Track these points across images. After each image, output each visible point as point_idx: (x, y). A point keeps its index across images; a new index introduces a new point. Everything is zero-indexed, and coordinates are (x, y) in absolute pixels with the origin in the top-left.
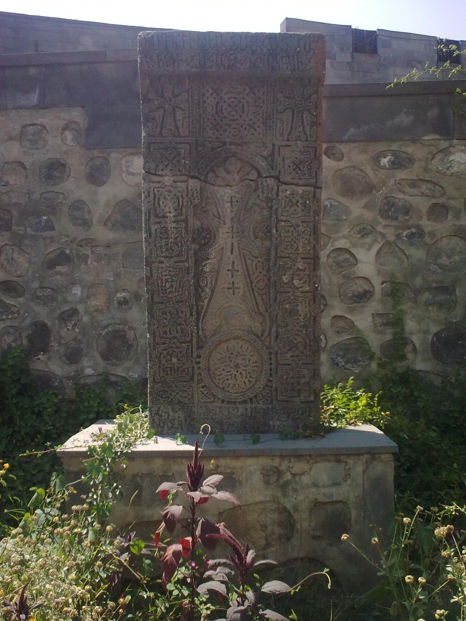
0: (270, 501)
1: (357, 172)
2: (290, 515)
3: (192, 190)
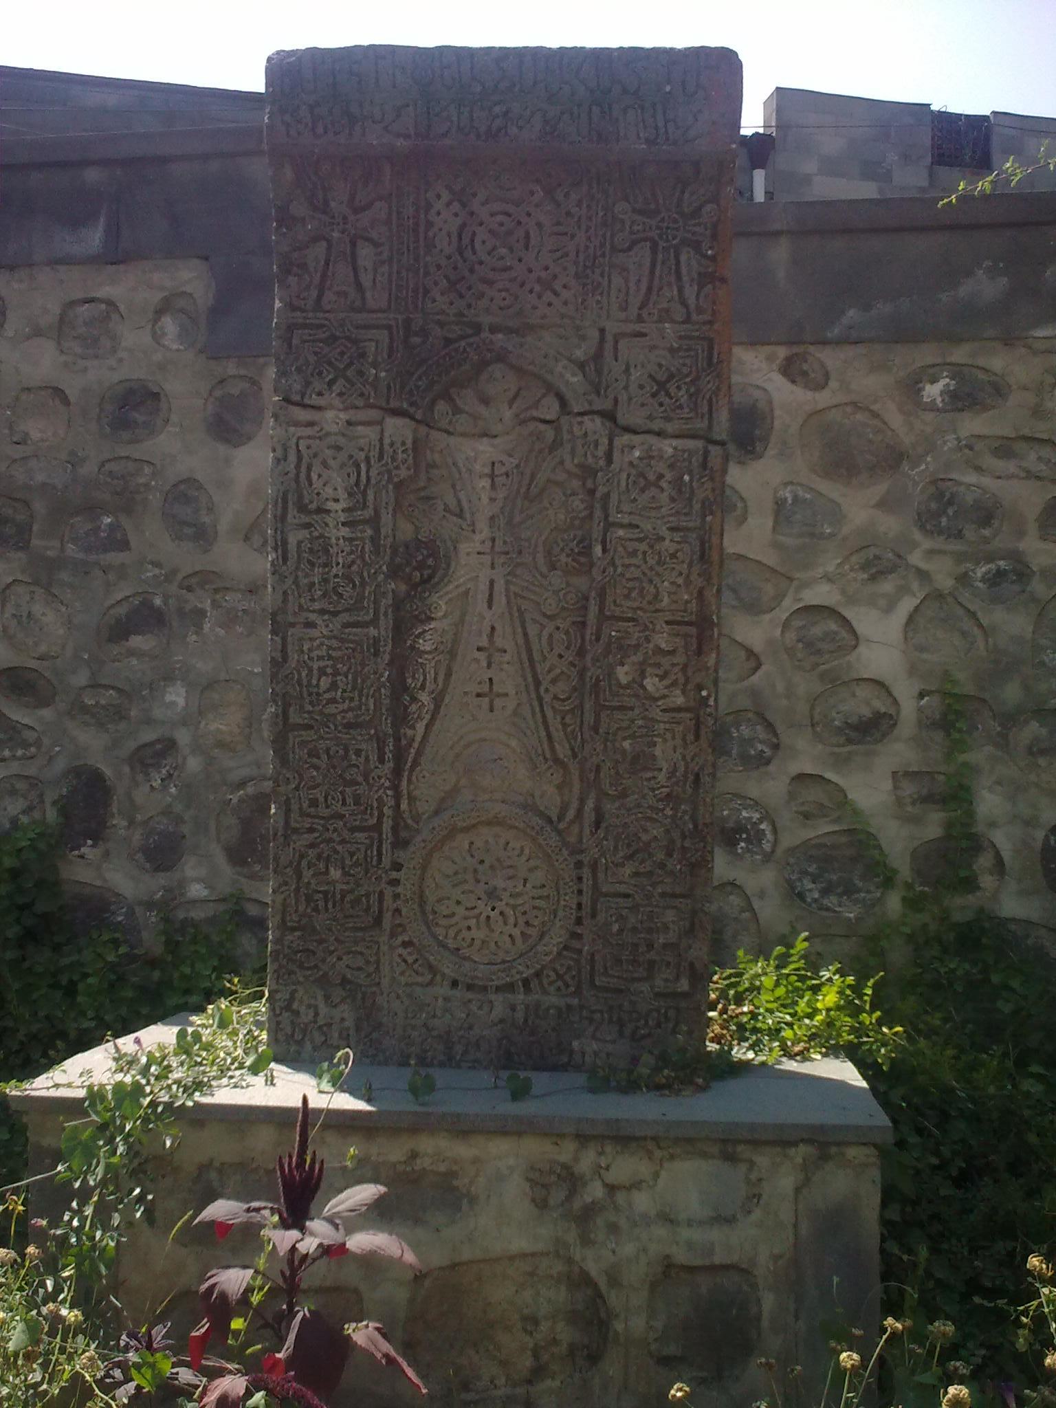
0: (547, 1254)
1: (859, 417)
2: (600, 1295)
3: (392, 445)
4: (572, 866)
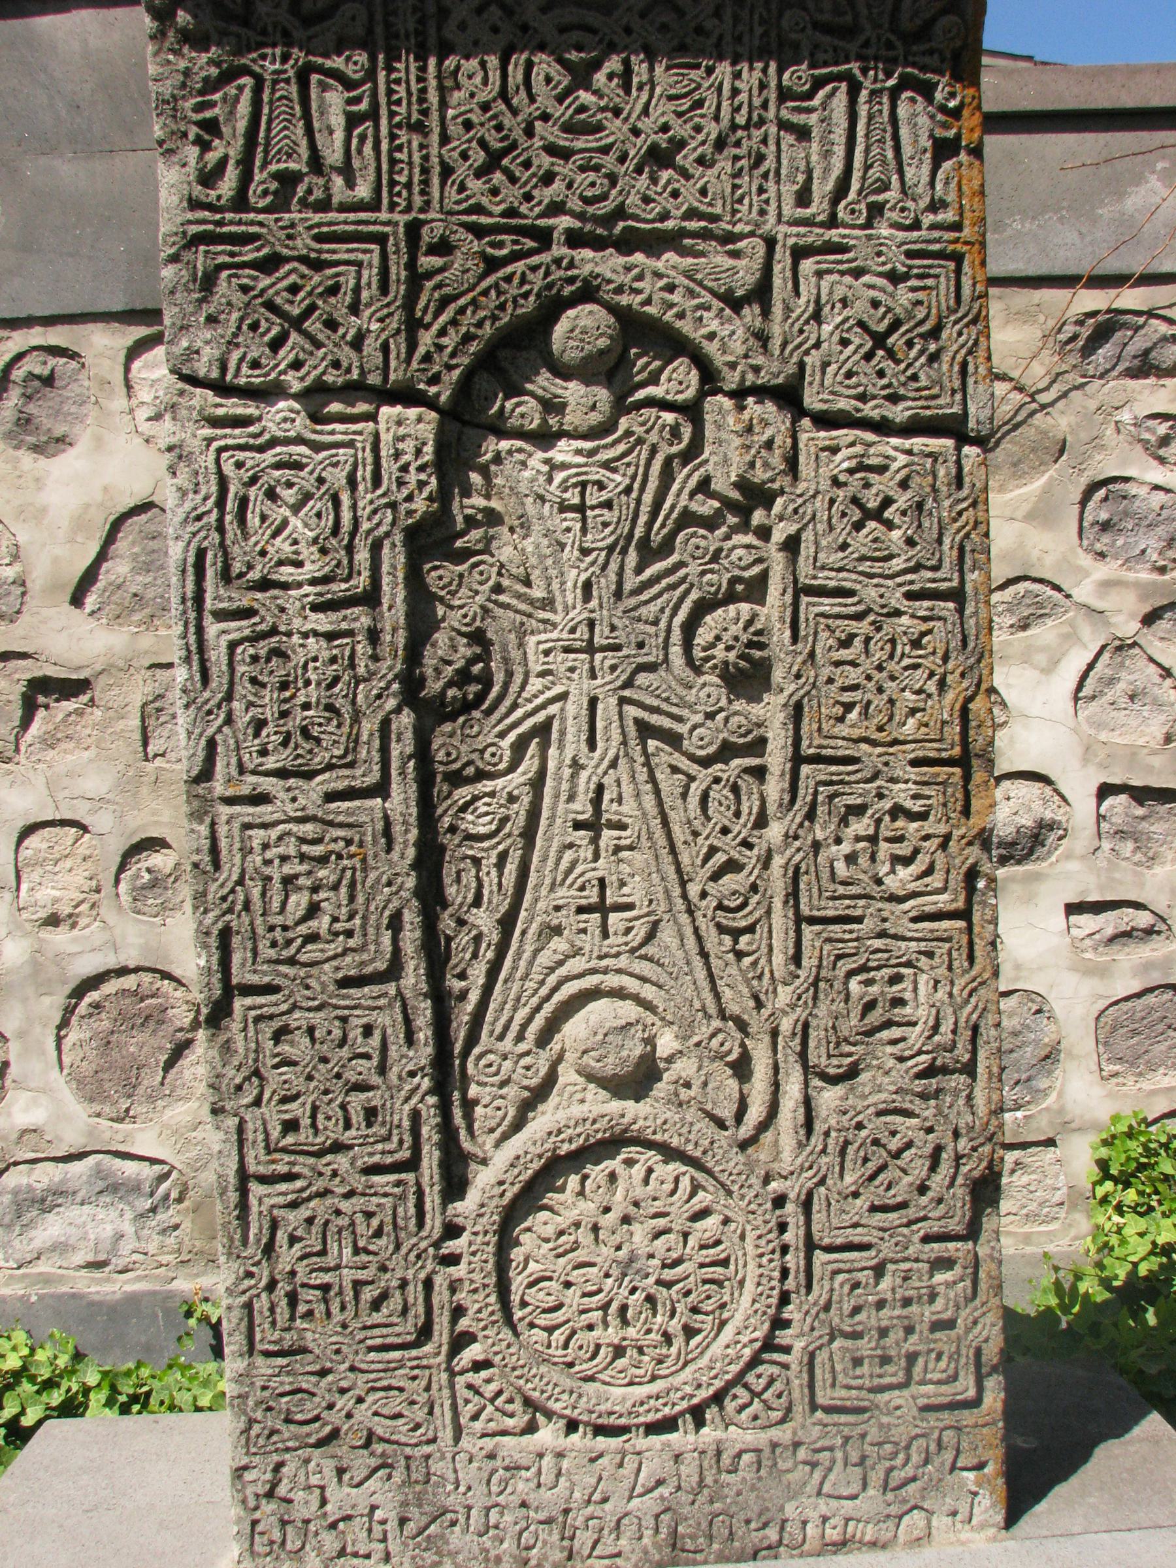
4: (769, 1205)
